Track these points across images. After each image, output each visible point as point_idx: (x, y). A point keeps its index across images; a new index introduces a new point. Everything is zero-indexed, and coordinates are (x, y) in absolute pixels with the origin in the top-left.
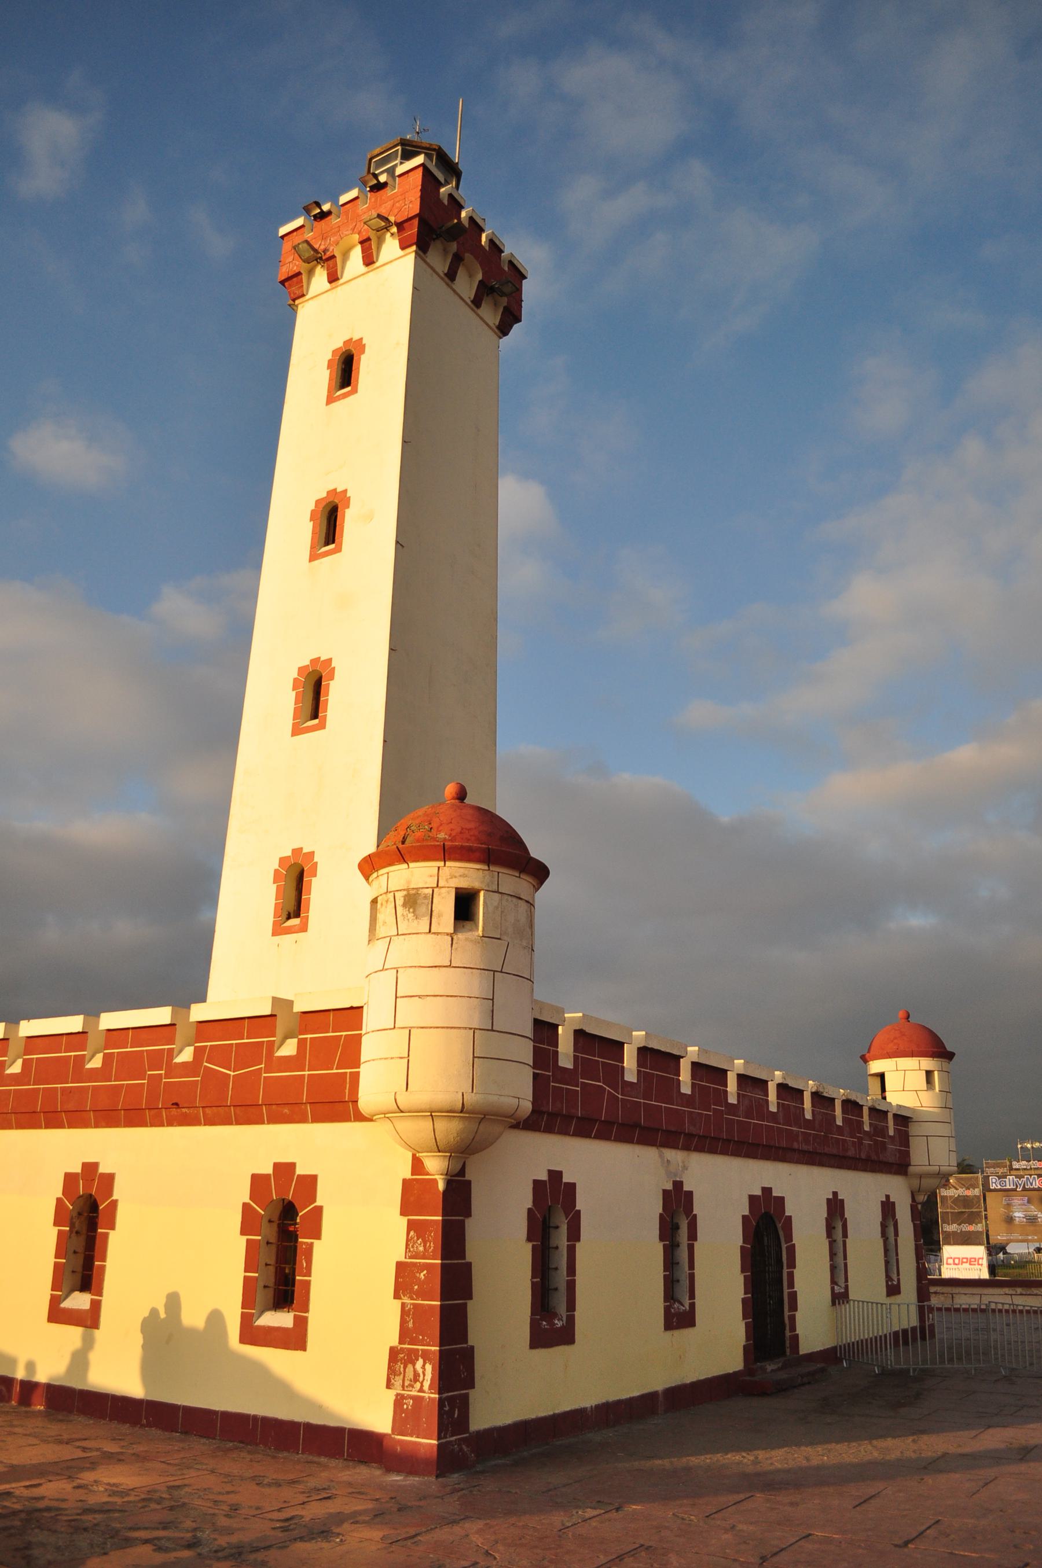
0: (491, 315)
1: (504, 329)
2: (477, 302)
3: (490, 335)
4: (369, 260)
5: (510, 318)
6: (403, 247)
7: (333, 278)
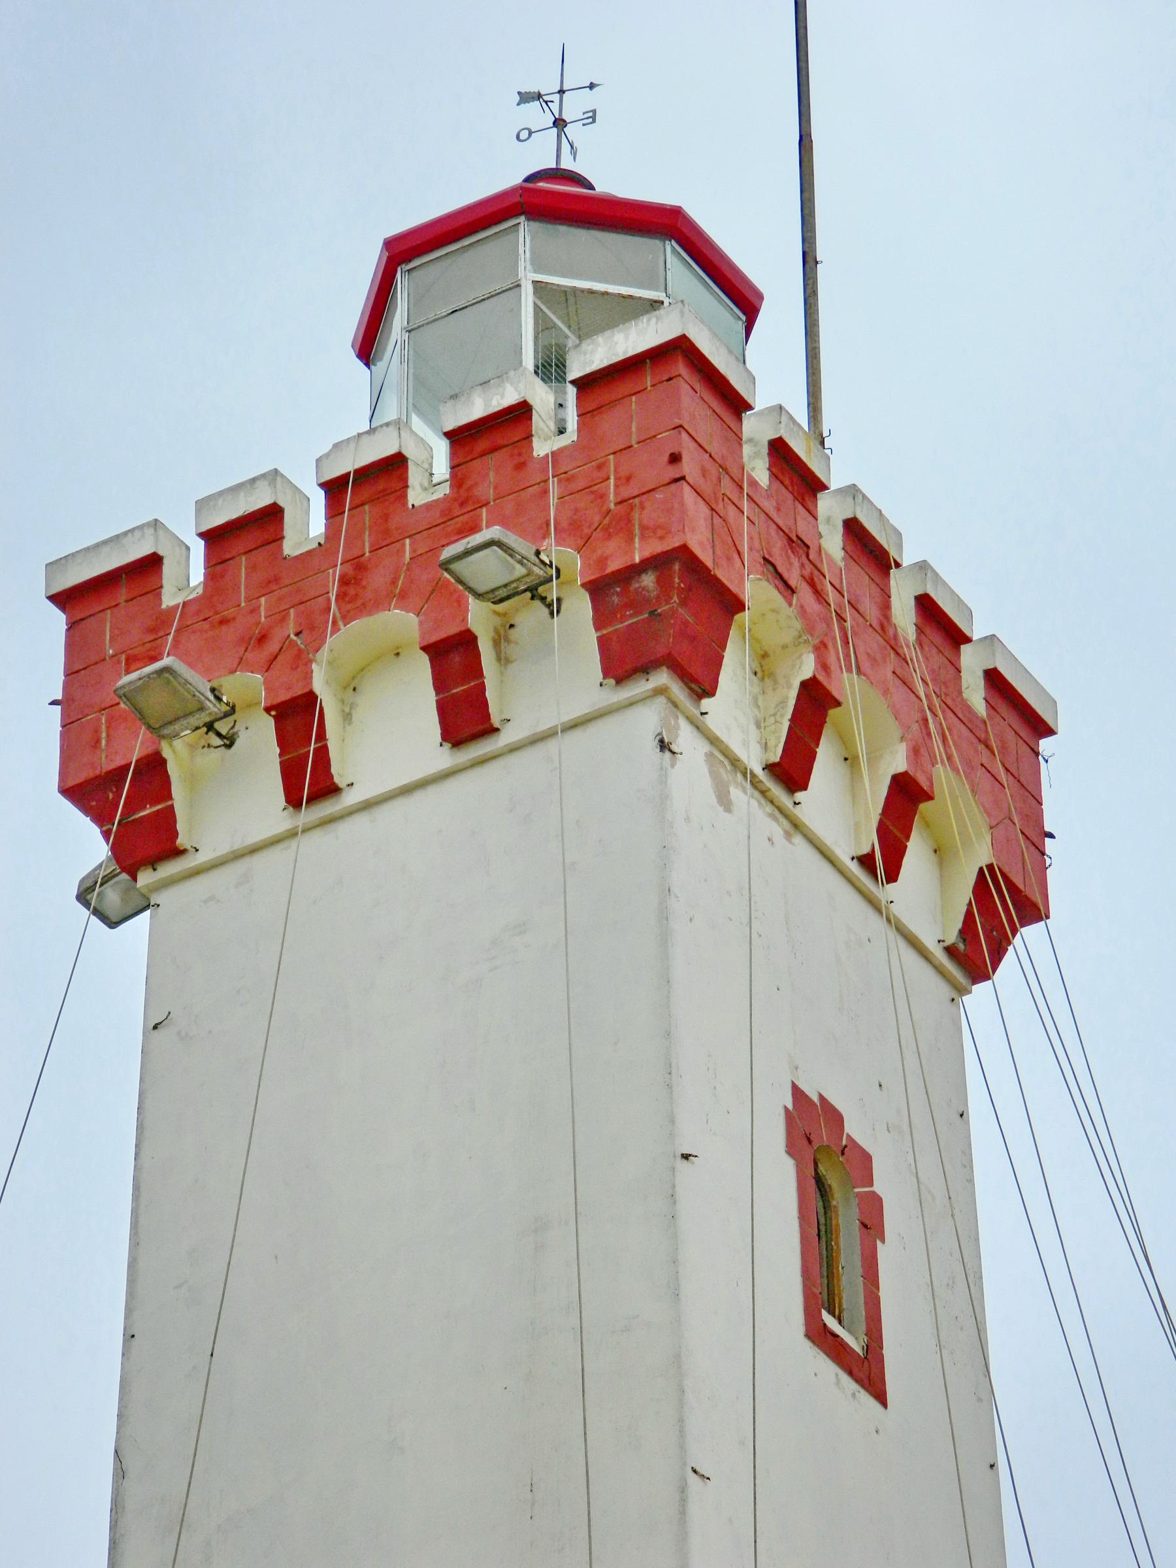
0: (927, 893)
1: (976, 951)
3: (927, 985)
5: (1000, 911)
6: (622, 663)
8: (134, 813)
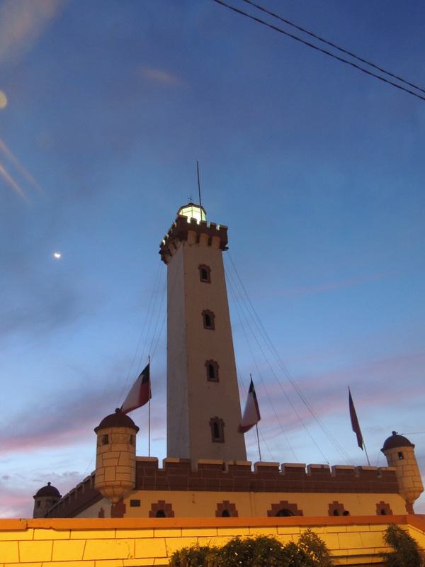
2: (198, 241)
4: (176, 248)
5: (223, 246)
7: (171, 255)
8: (164, 259)
